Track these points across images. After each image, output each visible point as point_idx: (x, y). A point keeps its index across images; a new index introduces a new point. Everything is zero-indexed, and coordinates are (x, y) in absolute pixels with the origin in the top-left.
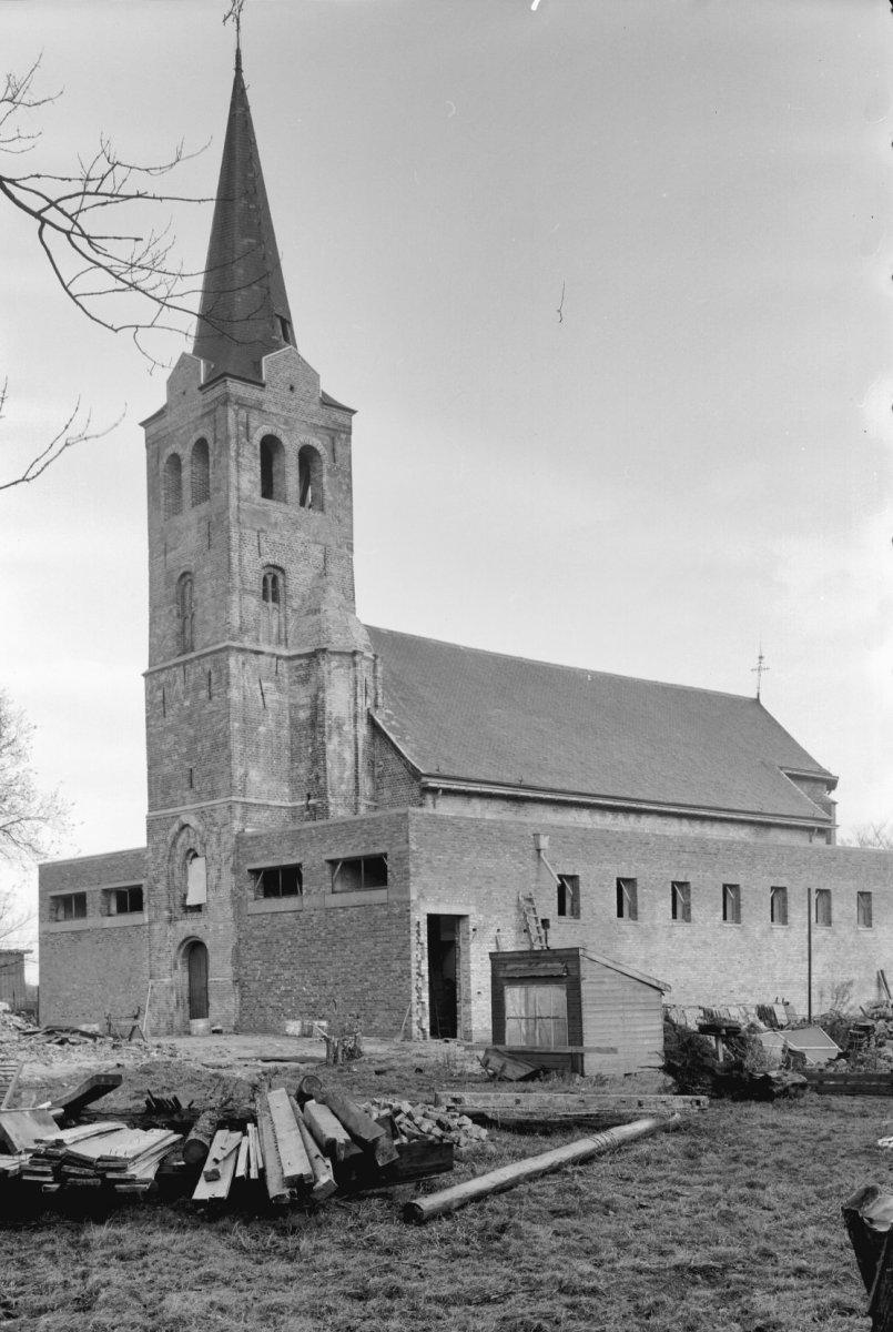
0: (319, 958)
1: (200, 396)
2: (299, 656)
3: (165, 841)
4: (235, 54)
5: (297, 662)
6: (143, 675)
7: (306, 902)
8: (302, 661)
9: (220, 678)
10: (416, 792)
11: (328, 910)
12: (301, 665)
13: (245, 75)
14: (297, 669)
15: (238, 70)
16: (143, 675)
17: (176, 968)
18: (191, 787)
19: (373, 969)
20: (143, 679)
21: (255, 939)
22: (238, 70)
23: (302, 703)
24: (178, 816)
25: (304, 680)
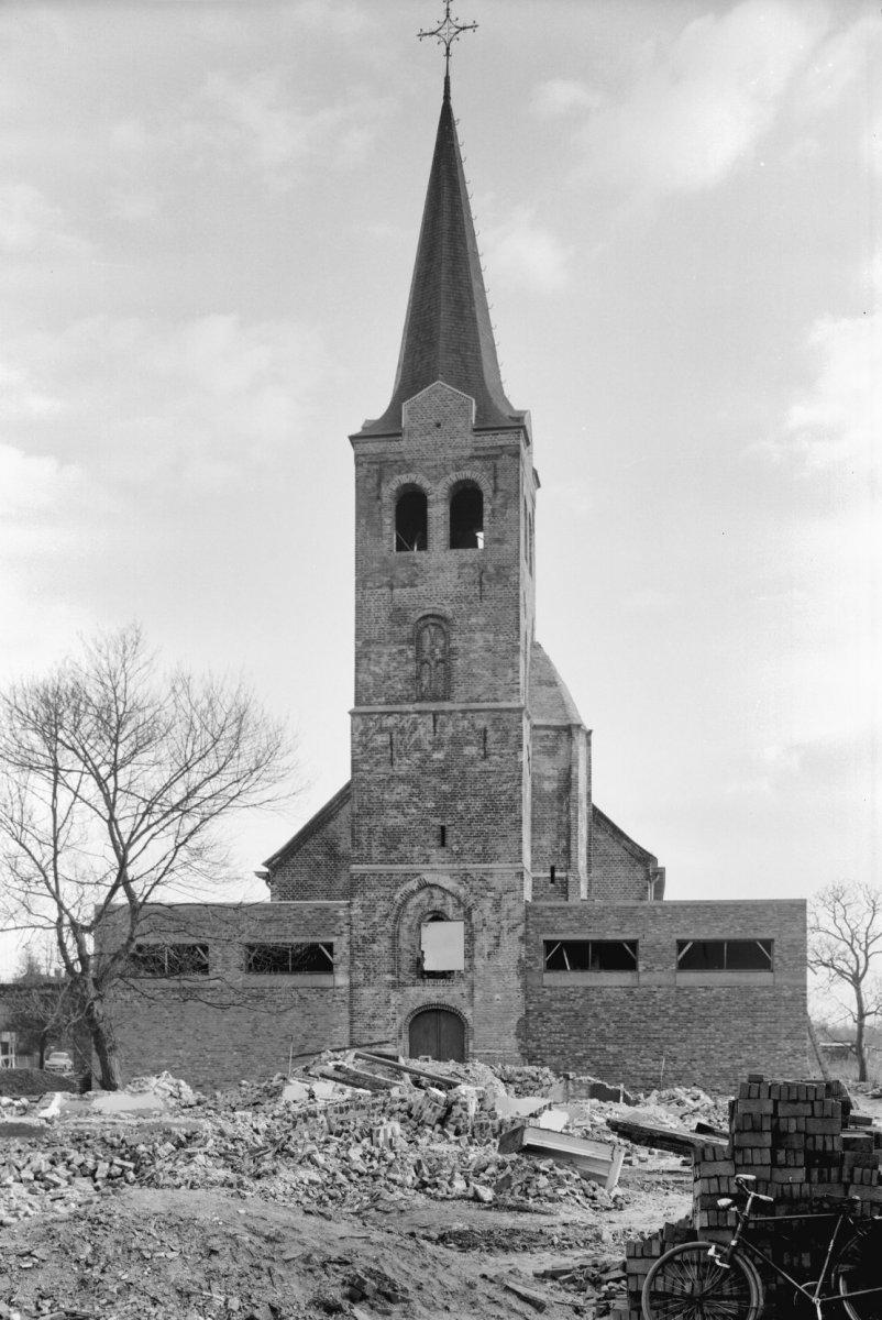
0: (664, 1034)
1: (471, 438)
2: (547, 727)
3: (391, 899)
4: (443, 82)
5: (543, 733)
6: (350, 713)
7: (644, 979)
8: (549, 732)
9: (503, 741)
10: (640, 875)
11: (679, 990)
12: (548, 736)
13: (453, 103)
14: (542, 739)
15: (447, 97)
16: (350, 713)
17: (400, 1037)
18: (443, 844)
19: (750, 1047)
20: (349, 716)
21: (554, 1012)
22: (447, 97)
23: (547, 774)
24: (418, 874)
25: (551, 752)
